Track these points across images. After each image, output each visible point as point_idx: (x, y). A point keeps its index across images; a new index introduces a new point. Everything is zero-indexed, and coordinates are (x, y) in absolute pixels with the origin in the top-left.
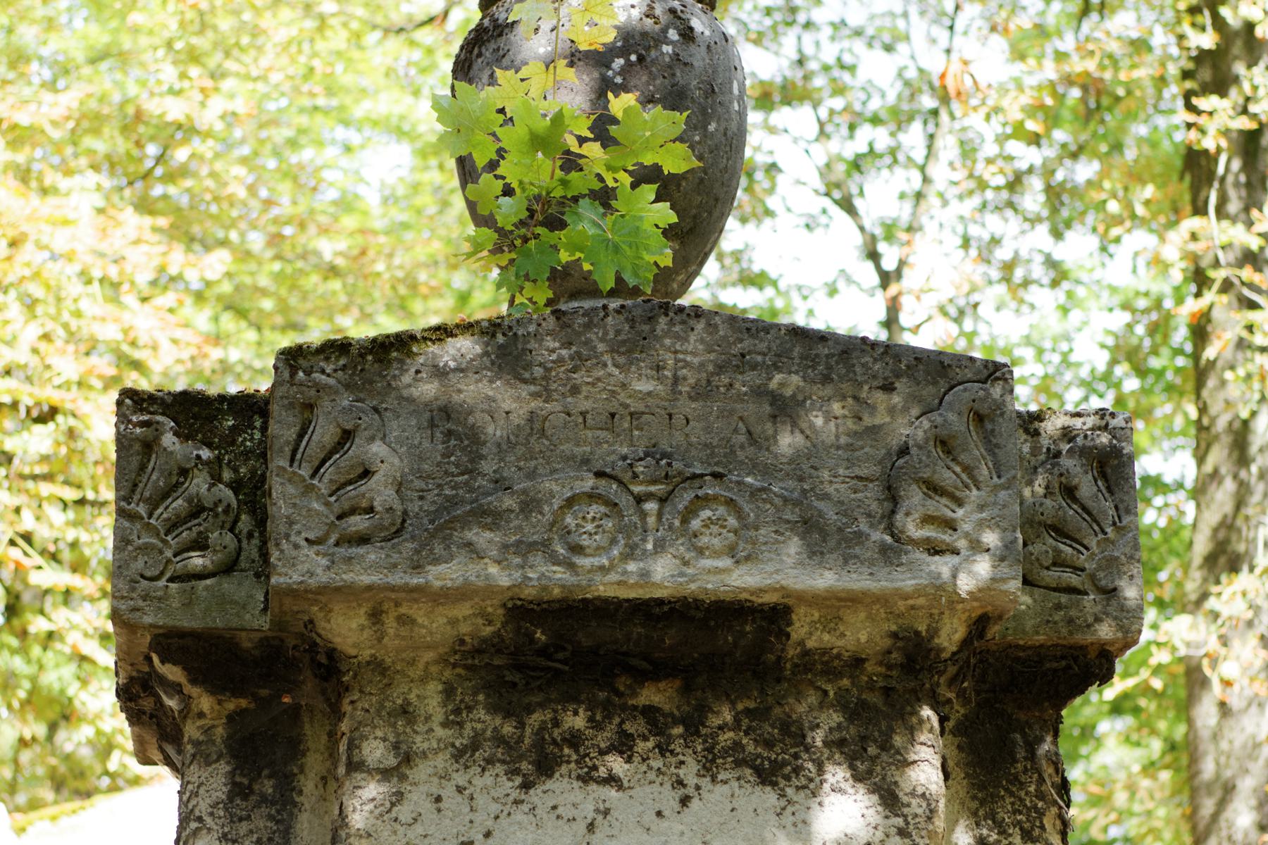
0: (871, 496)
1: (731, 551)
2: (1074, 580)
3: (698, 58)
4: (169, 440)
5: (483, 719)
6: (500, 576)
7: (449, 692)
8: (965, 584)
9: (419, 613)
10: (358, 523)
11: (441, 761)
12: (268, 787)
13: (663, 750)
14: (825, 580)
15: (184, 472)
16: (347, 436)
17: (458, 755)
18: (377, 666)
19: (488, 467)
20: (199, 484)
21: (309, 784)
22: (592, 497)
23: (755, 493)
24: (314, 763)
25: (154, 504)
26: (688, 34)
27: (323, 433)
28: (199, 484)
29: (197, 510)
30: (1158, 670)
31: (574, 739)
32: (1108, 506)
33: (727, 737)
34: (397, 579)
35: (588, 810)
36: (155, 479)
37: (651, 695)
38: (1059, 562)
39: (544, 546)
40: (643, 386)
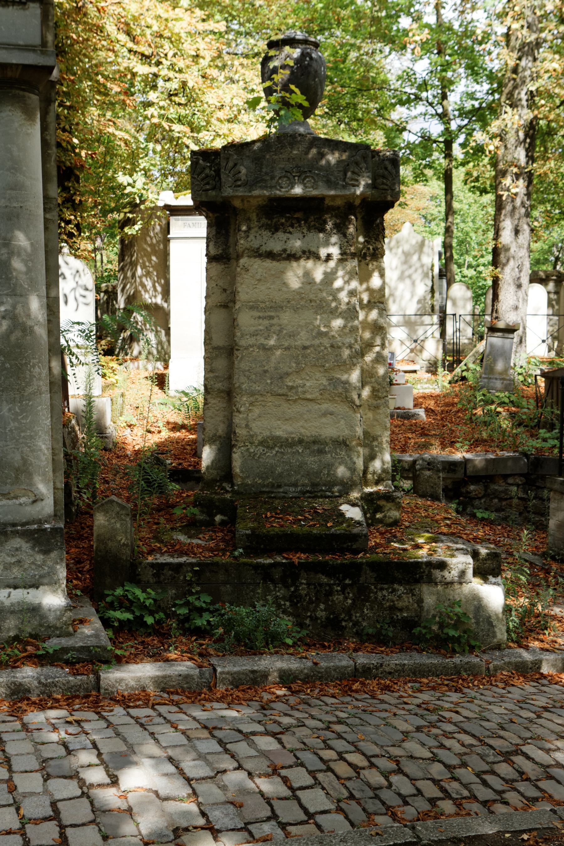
0: (341, 174)
1: (312, 187)
2: (386, 187)
3: (314, 64)
4: (201, 162)
5: (264, 220)
6: (267, 193)
7: (257, 215)
8: (358, 192)
9: (251, 200)
10: (239, 183)
11: (256, 229)
12: (224, 232)
13: (300, 226)
14: (332, 193)
15: (204, 168)
16: (235, 165)
17: (260, 228)
18: (243, 210)
19: (264, 170)
20: (207, 171)
21: (232, 231)
22: (285, 177)
23: (317, 175)
24: (232, 227)
25: (198, 175)
26: (311, 58)
27: (231, 164)
28: (207, 171)
29: (207, 176)
30: (472, 148)
31: (282, 224)
32: (394, 171)
33: (312, 223)
34: (246, 194)
35: (285, 238)
36: (199, 170)
37: (297, 215)
38: (383, 184)
39: (275, 187)
40: (295, 152)
